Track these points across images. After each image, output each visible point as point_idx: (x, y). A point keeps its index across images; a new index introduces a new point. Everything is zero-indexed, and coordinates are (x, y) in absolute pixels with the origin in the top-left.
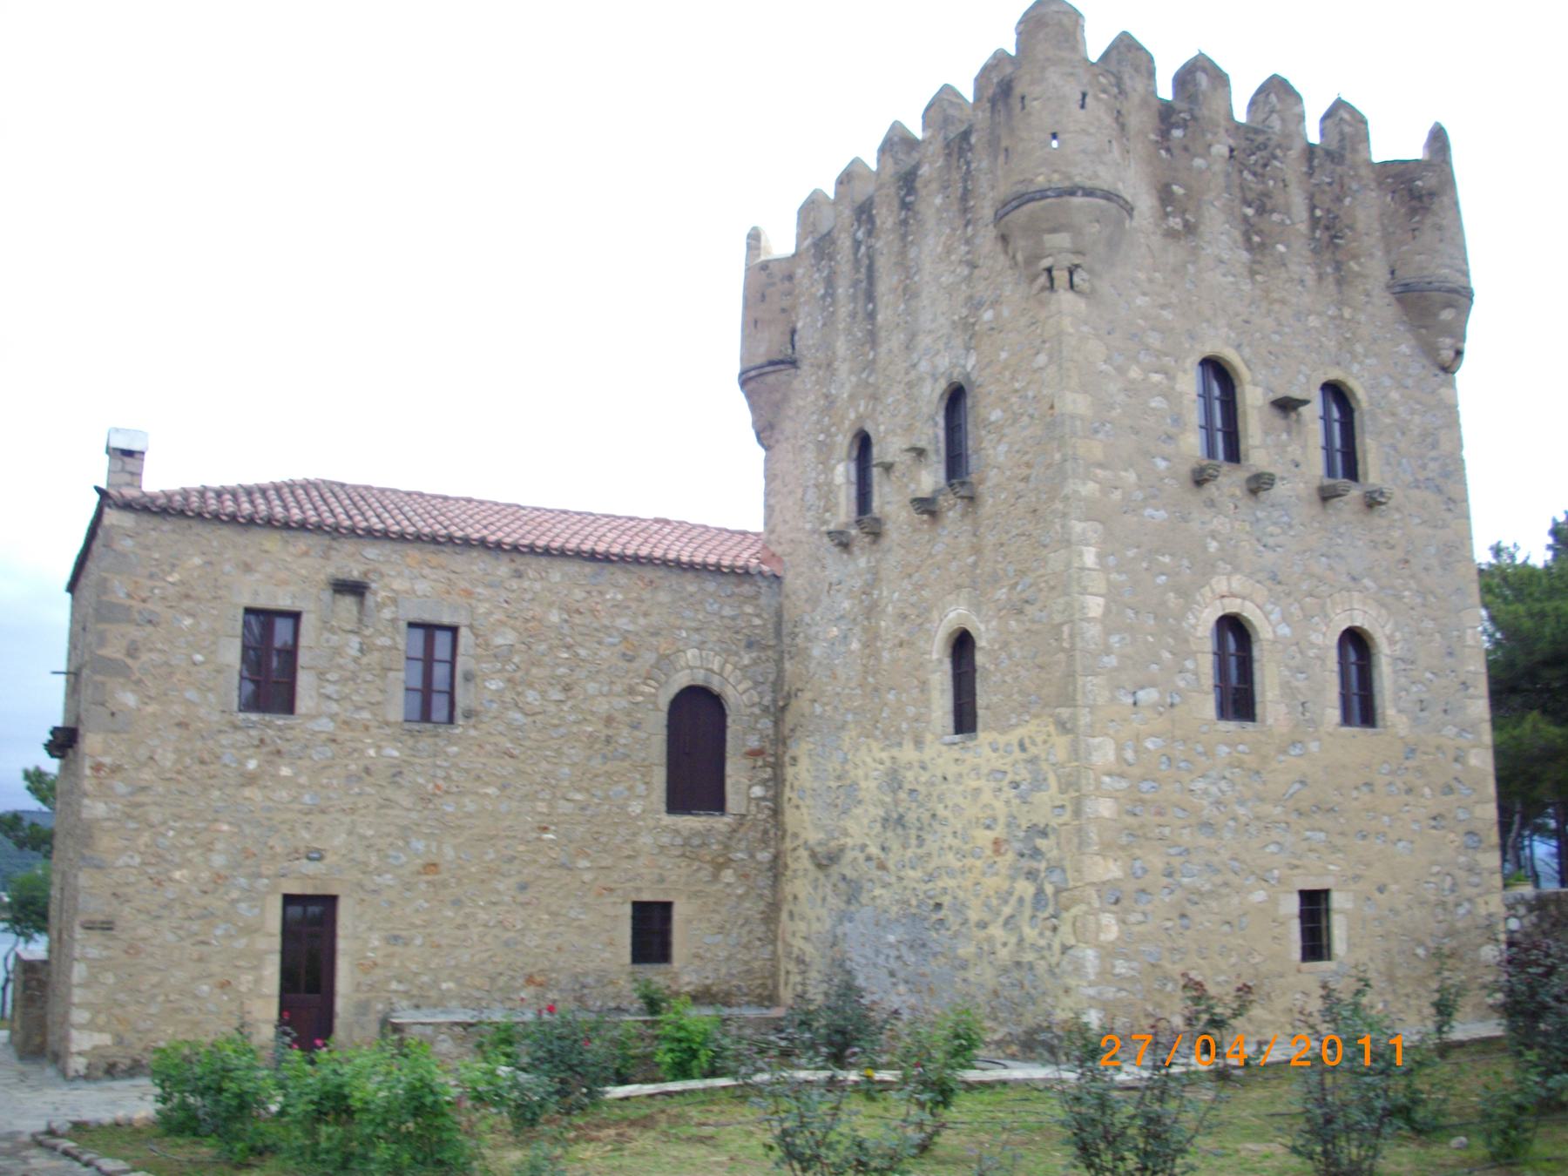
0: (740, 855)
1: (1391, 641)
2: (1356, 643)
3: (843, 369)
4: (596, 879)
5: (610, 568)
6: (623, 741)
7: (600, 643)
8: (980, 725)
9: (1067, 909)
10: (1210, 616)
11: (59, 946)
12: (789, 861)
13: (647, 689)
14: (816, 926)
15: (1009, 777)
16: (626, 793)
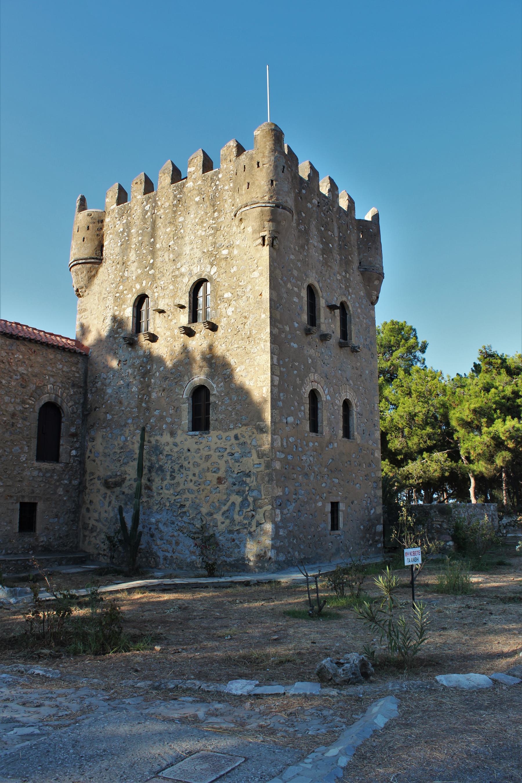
0: (66, 482)
1: (356, 406)
2: (347, 404)
3: (133, 267)
4: (4, 491)
5: (18, 342)
6: (19, 426)
7: (11, 378)
8: (211, 428)
9: (261, 508)
10: (308, 389)
11: (256, 514)
12: (87, 485)
13: (30, 402)
14: (104, 515)
15: (228, 451)
16: (20, 451)
